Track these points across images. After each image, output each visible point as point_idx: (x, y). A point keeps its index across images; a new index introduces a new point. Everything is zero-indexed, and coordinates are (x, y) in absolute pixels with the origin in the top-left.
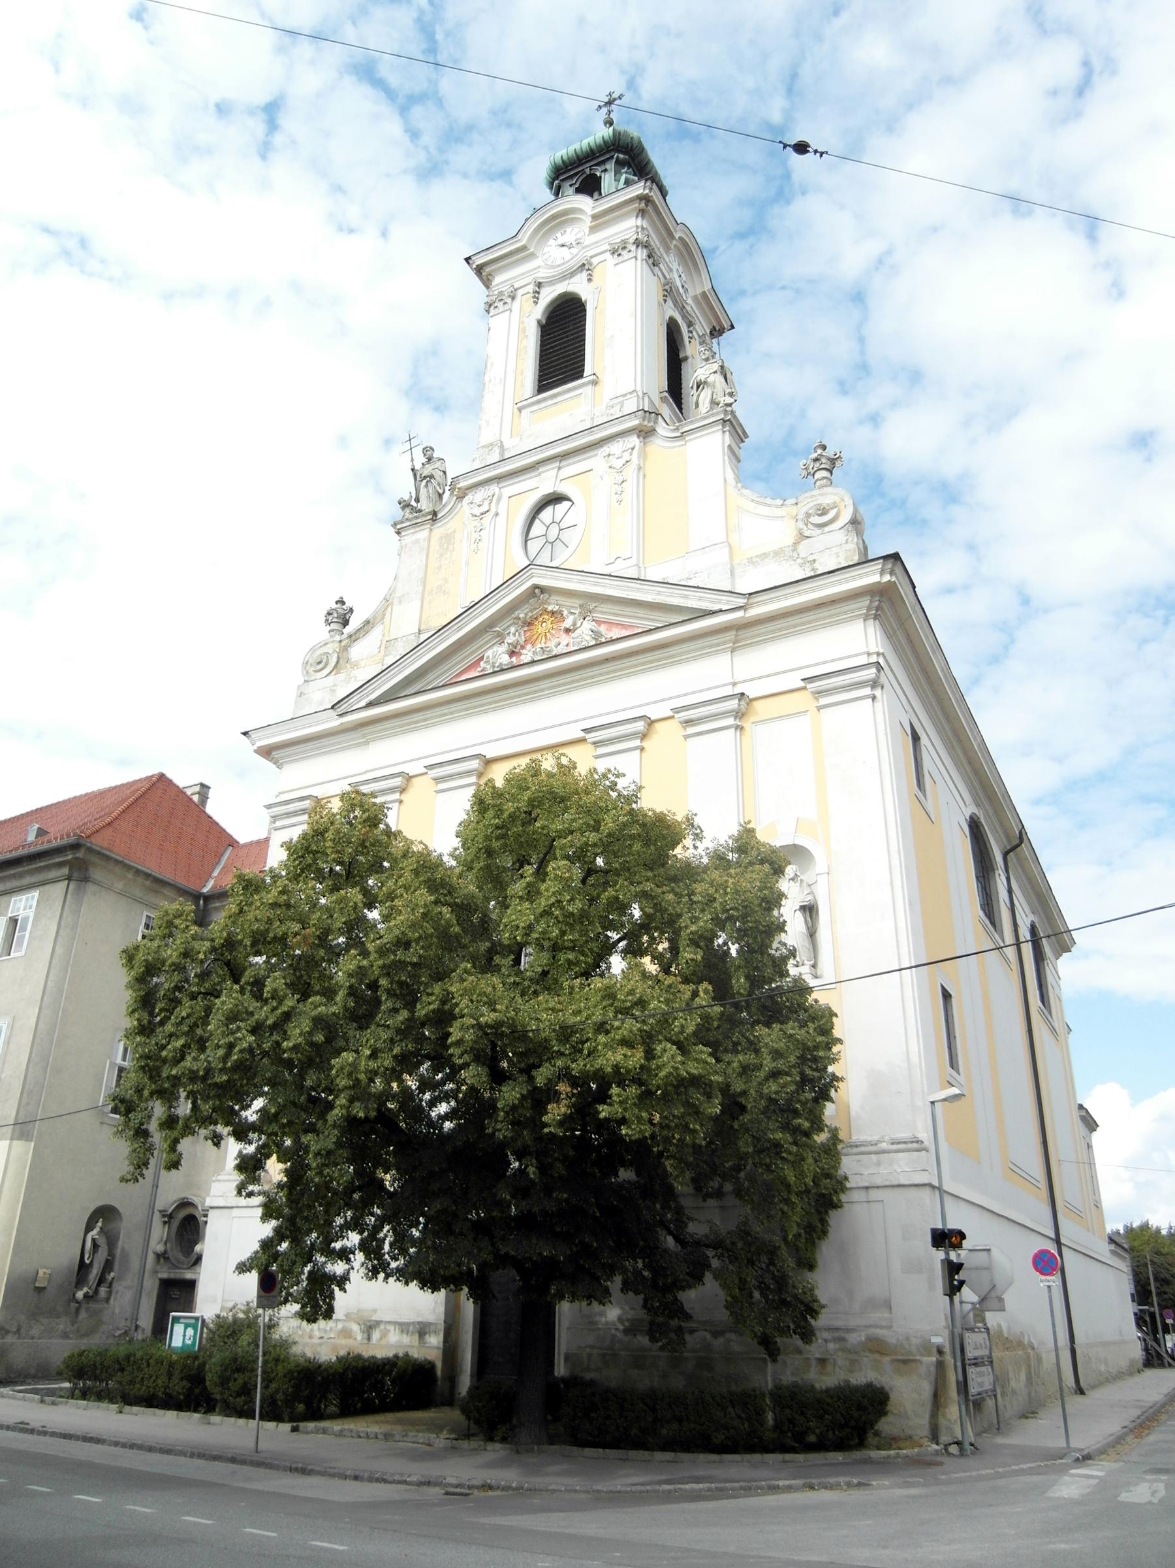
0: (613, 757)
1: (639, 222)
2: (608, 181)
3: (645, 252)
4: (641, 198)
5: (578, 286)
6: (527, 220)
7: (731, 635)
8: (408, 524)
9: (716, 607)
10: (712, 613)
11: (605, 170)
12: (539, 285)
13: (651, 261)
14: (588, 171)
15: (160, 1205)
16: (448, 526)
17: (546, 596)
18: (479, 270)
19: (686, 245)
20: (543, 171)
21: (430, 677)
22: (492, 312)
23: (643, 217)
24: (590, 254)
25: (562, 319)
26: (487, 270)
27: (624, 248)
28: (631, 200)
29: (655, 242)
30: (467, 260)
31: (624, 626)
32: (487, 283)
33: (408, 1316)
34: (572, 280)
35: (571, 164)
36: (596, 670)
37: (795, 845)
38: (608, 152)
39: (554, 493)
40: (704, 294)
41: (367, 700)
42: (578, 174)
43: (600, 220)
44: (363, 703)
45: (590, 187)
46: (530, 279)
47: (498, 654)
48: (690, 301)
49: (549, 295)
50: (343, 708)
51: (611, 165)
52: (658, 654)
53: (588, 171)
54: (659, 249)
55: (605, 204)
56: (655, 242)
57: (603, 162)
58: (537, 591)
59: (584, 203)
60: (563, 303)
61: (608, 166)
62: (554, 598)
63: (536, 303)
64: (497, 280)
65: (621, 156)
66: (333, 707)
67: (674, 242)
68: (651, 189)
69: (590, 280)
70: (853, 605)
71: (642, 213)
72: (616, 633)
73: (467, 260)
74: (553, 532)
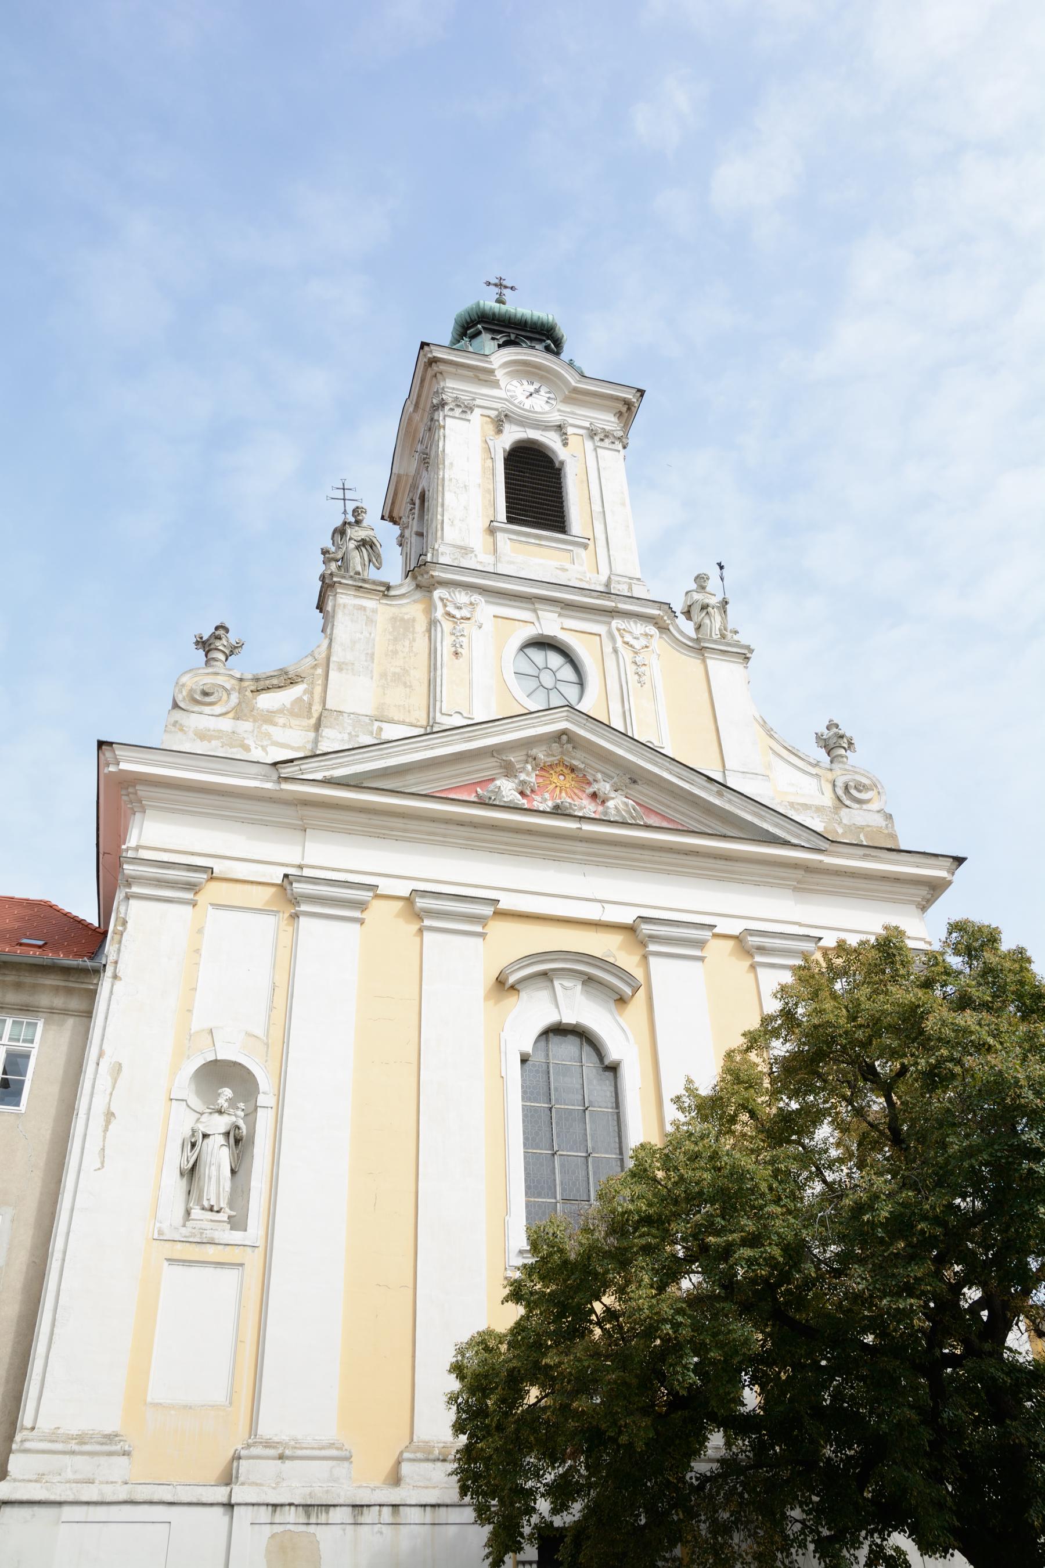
7: (800, 874)
8: (350, 582)
9: (794, 841)
10: (786, 843)
15: (303, 1519)
16: (404, 610)
17: (569, 746)
21: (411, 779)
24: (571, 421)
25: (532, 464)
26: (442, 367)
28: (617, 399)
30: (423, 345)
31: (664, 818)
35: (498, 320)
36: (647, 855)
37: (216, 1061)
38: (544, 335)
39: (553, 638)
41: (328, 774)
44: (319, 776)
47: (507, 789)
50: (287, 771)
52: (720, 864)
58: (564, 737)
60: (520, 448)
62: (579, 754)
66: (275, 764)
70: (912, 890)
72: (653, 821)
74: (547, 679)
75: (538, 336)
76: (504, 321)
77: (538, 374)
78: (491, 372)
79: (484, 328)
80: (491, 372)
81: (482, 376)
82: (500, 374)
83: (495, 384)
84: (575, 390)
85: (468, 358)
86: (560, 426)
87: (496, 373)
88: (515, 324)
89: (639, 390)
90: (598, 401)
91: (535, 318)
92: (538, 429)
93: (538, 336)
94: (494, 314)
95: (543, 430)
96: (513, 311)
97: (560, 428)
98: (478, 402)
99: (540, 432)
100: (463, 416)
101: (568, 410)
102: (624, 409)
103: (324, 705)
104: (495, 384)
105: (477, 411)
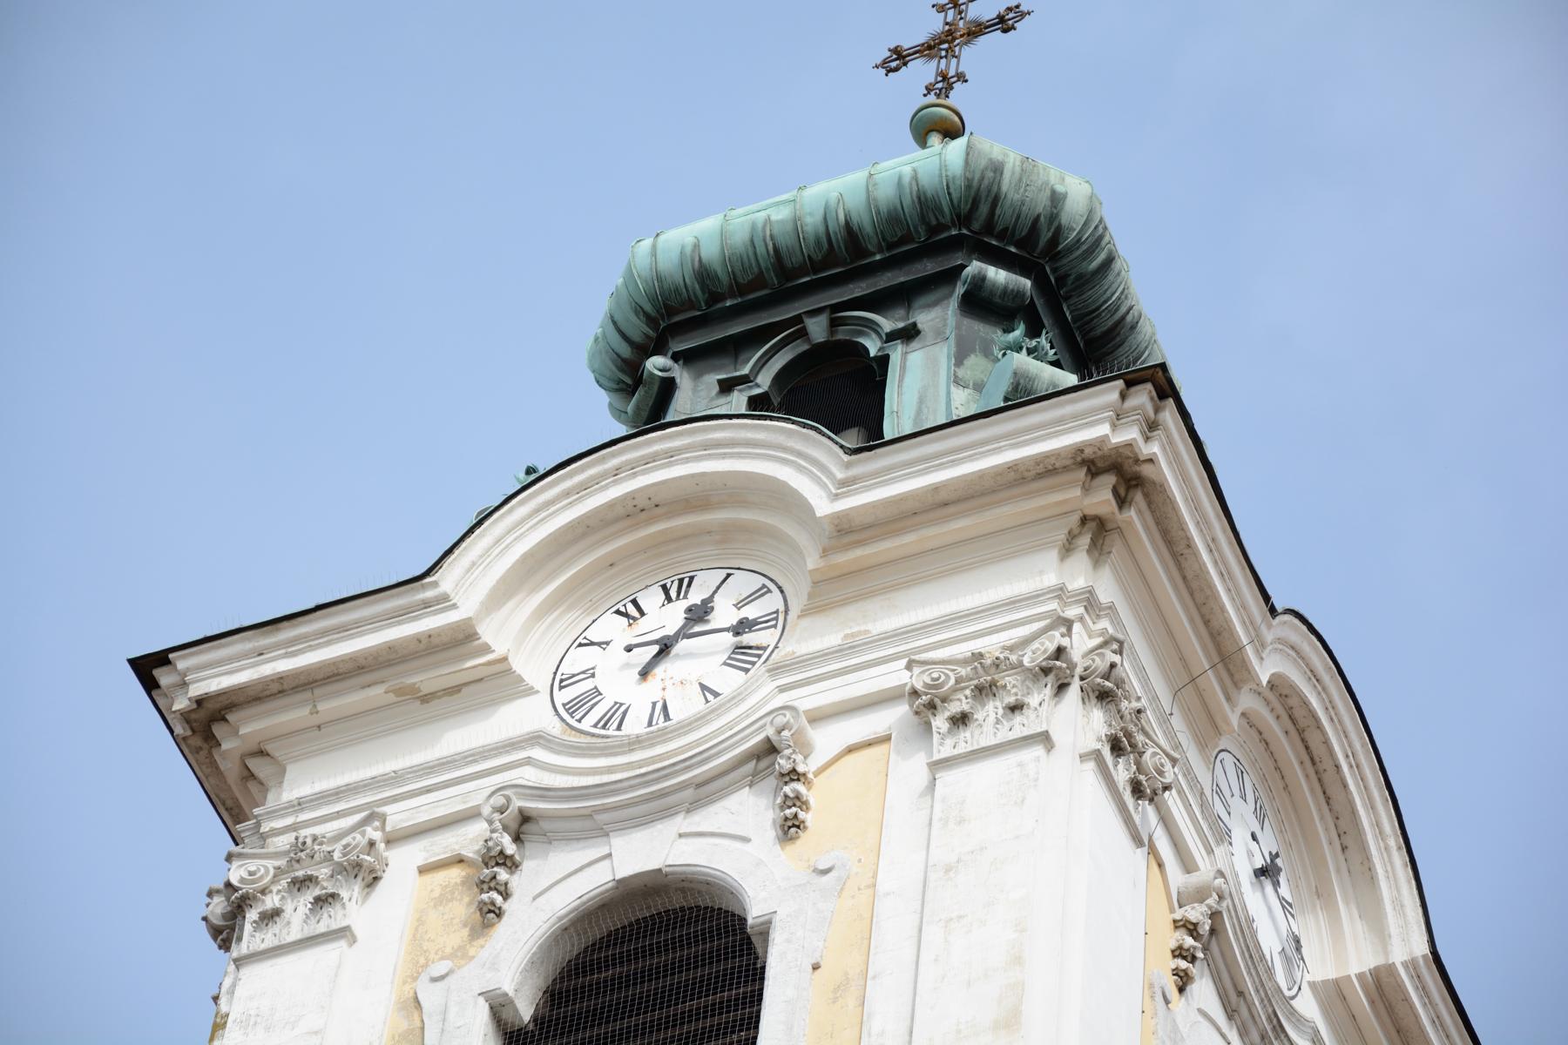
0: (1420, 910)
1: (1079, 574)
2: (924, 376)
3: (1093, 725)
4: (1093, 463)
5: (729, 846)
6: (535, 477)
11: (909, 334)
12: (523, 826)
13: (1122, 773)
14: (818, 329)
18: (201, 728)
19: (1300, 724)
20: (585, 314)
22: (251, 939)
23: (1098, 549)
26: (250, 727)
27: (984, 691)
28: (1046, 470)
29: (1146, 680)
30: (147, 668)
32: (233, 805)
33: (1259, 894)
34: (707, 819)
35: (738, 288)
38: (955, 244)
40: (1381, 984)
42: (784, 328)
43: (861, 557)
45: (840, 396)
46: (477, 793)
48: (1307, 1005)
49: (557, 888)
51: (939, 317)
53: (818, 329)
54: (1167, 734)
55: (893, 480)
56: (1146, 680)
57: (902, 296)
59: (801, 465)
61: (925, 318)
63: (491, 914)
64: (301, 782)
65: (998, 275)
67: (1247, 701)
68: (1152, 426)
69: (790, 827)
71: (1097, 533)
73: (147, 668)
75: (929, 267)
76: (758, 281)
77: (703, 532)
78: (463, 639)
79: (682, 357)
80: (463, 639)
81: (428, 679)
82: (499, 636)
83: (500, 682)
84: (846, 531)
85: (344, 631)
86: (770, 749)
87: (487, 632)
88: (814, 265)
89: (150, 685)
90: (908, 541)
91: (886, 194)
92: (666, 813)
93: (929, 267)
94: (704, 274)
95: (693, 806)
96: (781, 215)
97: (768, 760)
98: (399, 815)
99: (681, 823)
100: (326, 923)
101: (833, 640)
102: (1101, 498)
103: (1197, 689)
104: (500, 682)
105: (402, 862)
